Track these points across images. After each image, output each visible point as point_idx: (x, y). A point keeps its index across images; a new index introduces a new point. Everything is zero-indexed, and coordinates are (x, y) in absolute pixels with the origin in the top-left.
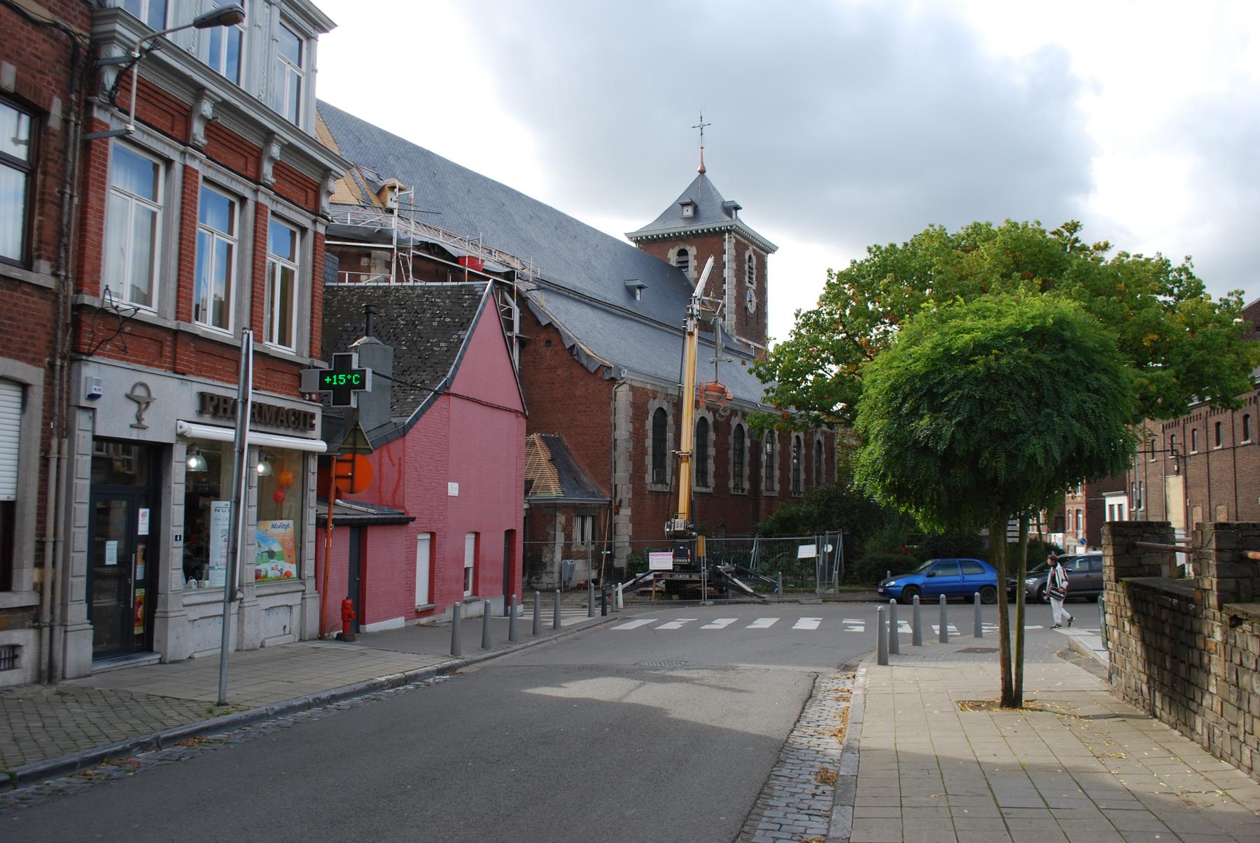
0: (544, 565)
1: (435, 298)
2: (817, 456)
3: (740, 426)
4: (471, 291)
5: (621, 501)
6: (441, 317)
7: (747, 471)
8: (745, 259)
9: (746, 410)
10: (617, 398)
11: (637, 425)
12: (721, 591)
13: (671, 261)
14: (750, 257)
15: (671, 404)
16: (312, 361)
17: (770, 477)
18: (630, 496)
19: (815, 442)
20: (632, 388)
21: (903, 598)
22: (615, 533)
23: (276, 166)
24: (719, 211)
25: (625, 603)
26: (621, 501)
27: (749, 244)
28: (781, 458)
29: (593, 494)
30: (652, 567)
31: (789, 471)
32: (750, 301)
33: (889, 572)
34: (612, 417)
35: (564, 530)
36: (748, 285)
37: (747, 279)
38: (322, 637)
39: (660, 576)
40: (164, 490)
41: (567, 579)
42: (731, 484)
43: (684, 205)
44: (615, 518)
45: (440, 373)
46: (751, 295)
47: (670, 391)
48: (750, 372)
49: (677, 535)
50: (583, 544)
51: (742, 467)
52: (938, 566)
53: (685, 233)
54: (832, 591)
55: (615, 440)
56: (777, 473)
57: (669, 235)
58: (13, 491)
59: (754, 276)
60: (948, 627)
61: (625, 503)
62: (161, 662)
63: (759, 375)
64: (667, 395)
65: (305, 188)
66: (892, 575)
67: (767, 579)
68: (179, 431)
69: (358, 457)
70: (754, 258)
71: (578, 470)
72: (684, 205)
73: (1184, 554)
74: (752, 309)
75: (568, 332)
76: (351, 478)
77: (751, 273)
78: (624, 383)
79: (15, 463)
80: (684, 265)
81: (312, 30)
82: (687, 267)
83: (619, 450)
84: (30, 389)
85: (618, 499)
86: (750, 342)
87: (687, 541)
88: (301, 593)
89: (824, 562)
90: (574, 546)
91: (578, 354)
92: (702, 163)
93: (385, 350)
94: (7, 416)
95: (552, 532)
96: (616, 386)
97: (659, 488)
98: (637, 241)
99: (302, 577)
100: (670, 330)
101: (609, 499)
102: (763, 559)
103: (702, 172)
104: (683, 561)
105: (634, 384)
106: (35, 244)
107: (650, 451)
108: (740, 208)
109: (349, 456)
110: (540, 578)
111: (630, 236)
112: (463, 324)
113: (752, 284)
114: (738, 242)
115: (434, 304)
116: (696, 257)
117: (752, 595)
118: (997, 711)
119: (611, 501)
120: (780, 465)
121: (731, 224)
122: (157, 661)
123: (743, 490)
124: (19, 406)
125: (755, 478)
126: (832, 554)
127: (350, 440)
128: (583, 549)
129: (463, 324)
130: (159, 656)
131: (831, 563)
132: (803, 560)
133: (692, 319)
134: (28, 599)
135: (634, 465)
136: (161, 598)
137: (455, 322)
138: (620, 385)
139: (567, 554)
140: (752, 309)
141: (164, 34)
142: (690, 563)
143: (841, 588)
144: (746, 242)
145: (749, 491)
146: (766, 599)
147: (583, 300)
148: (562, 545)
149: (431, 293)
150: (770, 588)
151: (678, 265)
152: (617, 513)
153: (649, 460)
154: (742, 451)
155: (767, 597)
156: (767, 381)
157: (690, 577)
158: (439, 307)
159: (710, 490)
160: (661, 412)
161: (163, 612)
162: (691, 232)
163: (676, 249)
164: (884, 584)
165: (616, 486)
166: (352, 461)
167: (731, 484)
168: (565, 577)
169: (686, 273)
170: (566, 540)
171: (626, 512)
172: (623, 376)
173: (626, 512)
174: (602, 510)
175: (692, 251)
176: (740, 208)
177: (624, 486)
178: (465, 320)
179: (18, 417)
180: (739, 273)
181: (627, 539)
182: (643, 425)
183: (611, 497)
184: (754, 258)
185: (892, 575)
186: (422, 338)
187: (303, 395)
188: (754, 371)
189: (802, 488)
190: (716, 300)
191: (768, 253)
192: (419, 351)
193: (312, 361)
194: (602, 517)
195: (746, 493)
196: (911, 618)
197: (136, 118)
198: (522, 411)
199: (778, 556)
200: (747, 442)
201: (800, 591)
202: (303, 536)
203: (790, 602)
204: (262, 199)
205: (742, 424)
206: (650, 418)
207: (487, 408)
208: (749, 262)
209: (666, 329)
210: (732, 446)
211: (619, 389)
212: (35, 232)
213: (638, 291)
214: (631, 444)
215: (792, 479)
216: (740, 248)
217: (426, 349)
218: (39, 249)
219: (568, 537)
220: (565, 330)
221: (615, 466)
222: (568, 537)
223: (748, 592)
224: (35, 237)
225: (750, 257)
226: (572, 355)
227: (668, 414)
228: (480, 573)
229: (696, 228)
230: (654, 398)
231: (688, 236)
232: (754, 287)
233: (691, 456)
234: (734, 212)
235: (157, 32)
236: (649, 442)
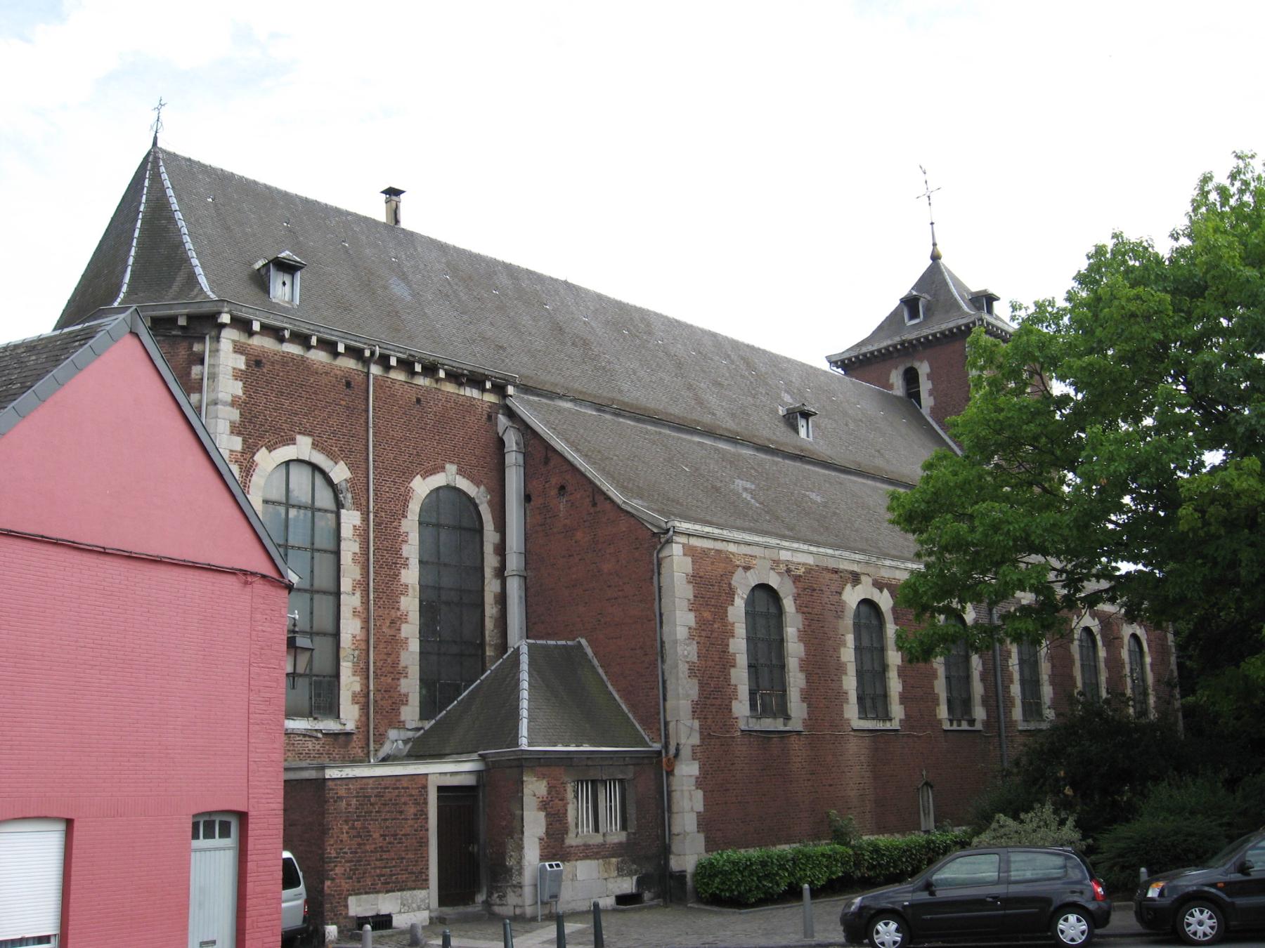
0: (508, 871)
5: (678, 750)
19: (1126, 639)
33: (1143, 870)
35: (544, 806)
61: (686, 752)
85: (672, 751)
92: (934, 245)
95: (518, 812)
103: (935, 257)
110: (505, 896)
111: (833, 362)
116: (930, 377)
135: (702, 686)
139: (555, 848)
145: (987, 724)
159: (895, 725)
163: (901, 369)
173: (687, 770)
175: (923, 369)
185: (1151, 872)
198: (268, 570)
227: (781, 595)
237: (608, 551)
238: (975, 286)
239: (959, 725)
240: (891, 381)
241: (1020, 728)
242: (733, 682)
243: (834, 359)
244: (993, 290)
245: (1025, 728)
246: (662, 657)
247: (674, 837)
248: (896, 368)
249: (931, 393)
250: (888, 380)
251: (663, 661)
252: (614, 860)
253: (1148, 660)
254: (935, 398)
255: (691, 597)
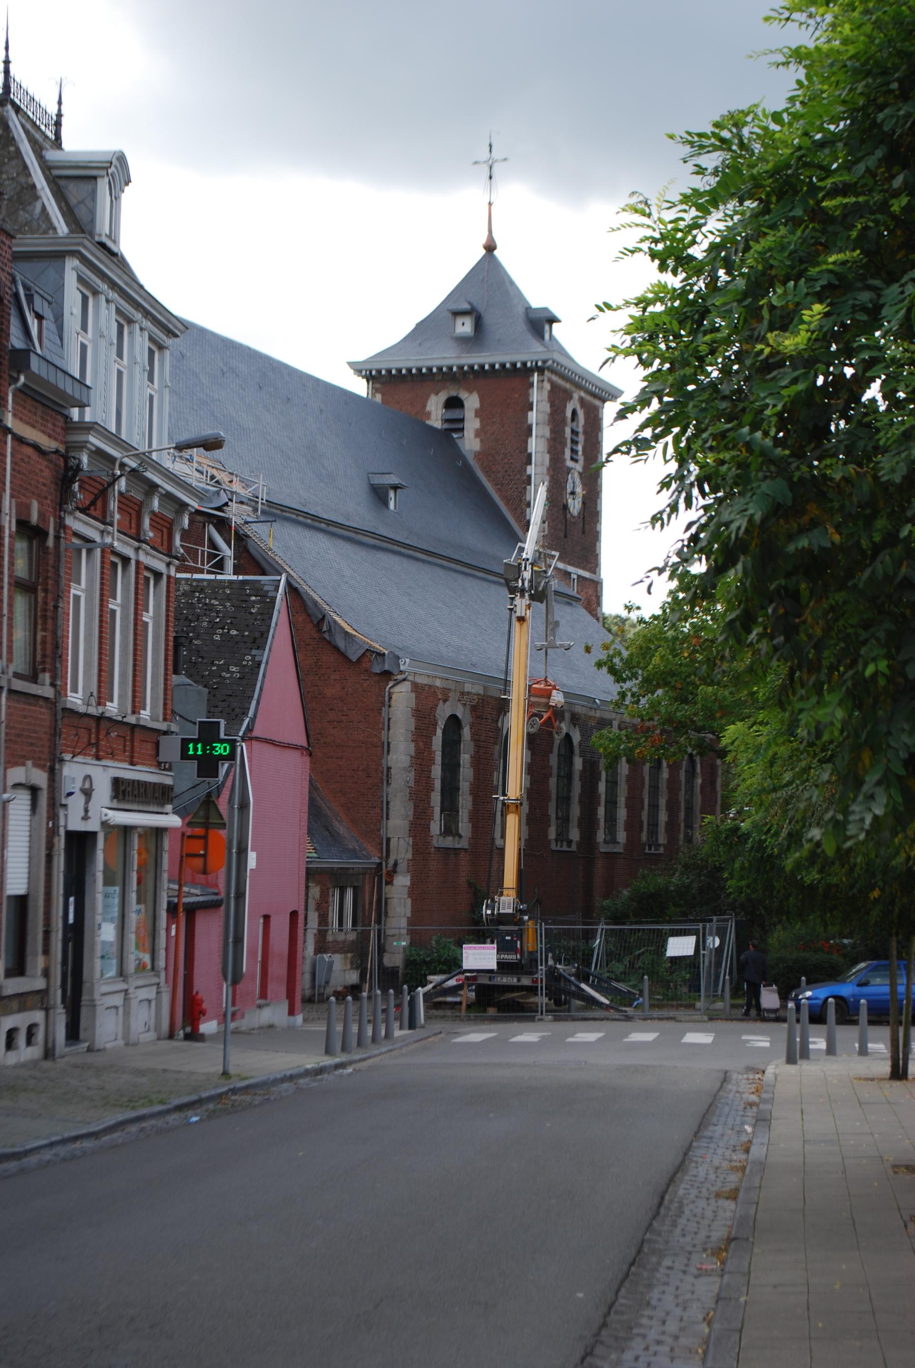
1: (210, 599)
2: (687, 782)
3: (568, 737)
4: (257, 589)
5: (396, 864)
6: (223, 628)
7: (576, 811)
8: (564, 418)
9: (578, 709)
10: (393, 703)
11: (421, 744)
12: (558, 1003)
13: (433, 416)
14: (574, 413)
15: (468, 707)
16: (169, 726)
17: (611, 819)
18: (410, 856)
20: (416, 687)
21: (818, 1017)
22: (386, 913)
23: (154, 518)
24: (521, 327)
25: (427, 1018)
26: (396, 864)
27: (573, 388)
28: (630, 789)
29: (354, 854)
30: (466, 965)
31: (642, 808)
32: (573, 493)
33: (803, 978)
34: (384, 732)
36: (569, 463)
37: (568, 453)
38: (171, 1036)
39: (474, 978)
40: (87, 878)
41: (323, 983)
42: (552, 833)
43: (457, 314)
44: (386, 889)
45: (237, 710)
46: (575, 484)
47: (468, 688)
48: (599, 665)
49: (503, 919)
50: (341, 930)
51: (568, 806)
52: (874, 969)
53: (461, 368)
54: (719, 1005)
55: (389, 769)
56: (622, 813)
57: (430, 369)
58: (26, 886)
59: (580, 448)
60: (870, 1045)
61: (403, 866)
62: (90, 1050)
63: (612, 671)
64: (462, 693)
65: (159, 527)
66: (809, 982)
67: (622, 986)
68: (104, 818)
69: (212, 833)
70: (581, 414)
71: (329, 813)
72: (457, 314)
73: (690, 952)
74: (575, 506)
75: (312, 593)
76: (204, 856)
77: (575, 442)
78: (404, 680)
79: (27, 860)
80: (456, 425)
81: (164, 337)
82: (462, 430)
83: (394, 785)
84: (39, 793)
85: (391, 862)
86: (570, 569)
87: (516, 928)
88: (155, 987)
89: (710, 963)
90: (330, 932)
91: (330, 631)
93: (199, 693)
94: (19, 818)
96: (391, 684)
97: (449, 842)
98: (369, 378)
99: (156, 968)
100: (445, 563)
101: (378, 861)
102: (610, 956)
103: (490, 248)
104: (510, 957)
105: (420, 680)
106: (39, 658)
107: (438, 784)
108: (558, 321)
109: (199, 831)
111: (358, 369)
112: (255, 639)
113: (576, 461)
114: (554, 387)
115: (210, 607)
116: (478, 413)
117: (607, 1008)
118: (887, 1085)
119: (380, 864)
120: (627, 799)
121: (544, 357)
122: (85, 1049)
123: (570, 843)
124: (29, 808)
125: (588, 823)
126: (719, 950)
127: (202, 813)
128: (341, 937)
129: (255, 639)
130: (87, 1044)
131: (718, 964)
132: (675, 960)
133: (522, 596)
134: (39, 984)
135: (416, 807)
136: (86, 987)
137: (243, 636)
138: (398, 683)
139: (322, 947)
140: (575, 506)
141: (150, 452)
142: (521, 960)
143: (733, 1002)
144: (568, 386)
145: (579, 844)
146: (628, 1013)
147: (317, 524)
148: (315, 931)
149: (202, 591)
150: (627, 999)
151: (446, 426)
152: (390, 882)
153: (436, 798)
154: (569, 777)
155: (630, 1011)
156: (624, 681)
157: (519, 980)
158: (218, 612)
160: (454, 722)
161: (89, 1000)
162: (471, 367)
163: (443, 397)
164: (797, 996)
165: (388, 840)
166: (205, 838)
167: (552, 833)
168: (320, 979)
169: (459, 442)
170: (320, 924)
171: (403, 881)
172: (402, 668)
173: (403, 881)
174: (367, 876)
175: (472, 402)
176: (558, 321)
177: (402, 841)
178: (257, 634)
179: (28, 818)
180: (555, 445)
181: (404, 923)
182: (428, 744)
183: (381, 858)
184: (581, 414)
185: (809, 982)
186: (203, 658)
187: (159, 764)
188: (605, 664)
189: (662, 839)
190: (548, 551)
191: (604, 401)
192: (203, 677)
193: (169, 726)
194: (367, 888)
195: (574, 848)
196: (825, 1034)
197: (119, 531)
199: (637, 952)
200: (578, 763)
201: (672, 1006)
202: (157, 923)
203: (660, 1019)
204: (143, 558)
205: (571, 734)
206: (439, 732)
207: (287, 750)
208: (573, 420)
209: (439, 561)
210: (555, 771)
211: (397, 689)
212: (39, 647)
213: (392, 494)
214: (412, 775)
215: (645, 824)
216: (558, 397)
217: (212, 674)
218: (43, 662)
219: (323, 919)
220: (307, 588)
221: (388, 808)
222: (323, 919)
223: (602, 1003)
224: (39, 651)
225: (574, 413)
226: (320, 631)
227: (463, 723)
228: (270, 970)
229: (480, 360)
230: (445, 701)
231: (465, 374)
232: (579, 467)
233: (521, 804)
234: (547, 327)
235: (141, 450)
236: (437, 771)
237: (332, 677)
238: (536, 301)
239: (561, 846)
240: (428, 409)
241: (602, 850)
242: (432, 805)
243: (359, 367)
244: (557, 312)
245: (607, 850)
246: (388, 781)
247: (389, 938)
248: (437, 394)
249: (478, 434)
250: (425, 406)
251: (388, 784)
252: (349, 955)
253: (699, 781)
254: (481, 441)
255: (413, 729)
